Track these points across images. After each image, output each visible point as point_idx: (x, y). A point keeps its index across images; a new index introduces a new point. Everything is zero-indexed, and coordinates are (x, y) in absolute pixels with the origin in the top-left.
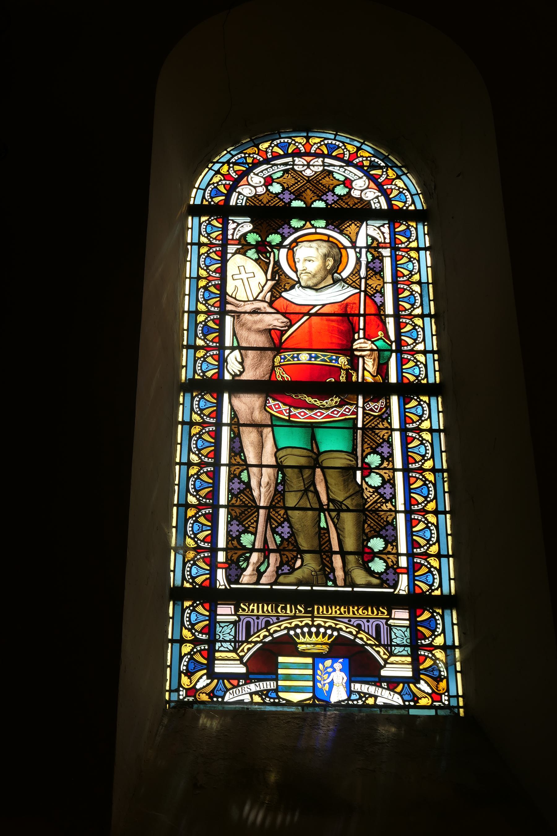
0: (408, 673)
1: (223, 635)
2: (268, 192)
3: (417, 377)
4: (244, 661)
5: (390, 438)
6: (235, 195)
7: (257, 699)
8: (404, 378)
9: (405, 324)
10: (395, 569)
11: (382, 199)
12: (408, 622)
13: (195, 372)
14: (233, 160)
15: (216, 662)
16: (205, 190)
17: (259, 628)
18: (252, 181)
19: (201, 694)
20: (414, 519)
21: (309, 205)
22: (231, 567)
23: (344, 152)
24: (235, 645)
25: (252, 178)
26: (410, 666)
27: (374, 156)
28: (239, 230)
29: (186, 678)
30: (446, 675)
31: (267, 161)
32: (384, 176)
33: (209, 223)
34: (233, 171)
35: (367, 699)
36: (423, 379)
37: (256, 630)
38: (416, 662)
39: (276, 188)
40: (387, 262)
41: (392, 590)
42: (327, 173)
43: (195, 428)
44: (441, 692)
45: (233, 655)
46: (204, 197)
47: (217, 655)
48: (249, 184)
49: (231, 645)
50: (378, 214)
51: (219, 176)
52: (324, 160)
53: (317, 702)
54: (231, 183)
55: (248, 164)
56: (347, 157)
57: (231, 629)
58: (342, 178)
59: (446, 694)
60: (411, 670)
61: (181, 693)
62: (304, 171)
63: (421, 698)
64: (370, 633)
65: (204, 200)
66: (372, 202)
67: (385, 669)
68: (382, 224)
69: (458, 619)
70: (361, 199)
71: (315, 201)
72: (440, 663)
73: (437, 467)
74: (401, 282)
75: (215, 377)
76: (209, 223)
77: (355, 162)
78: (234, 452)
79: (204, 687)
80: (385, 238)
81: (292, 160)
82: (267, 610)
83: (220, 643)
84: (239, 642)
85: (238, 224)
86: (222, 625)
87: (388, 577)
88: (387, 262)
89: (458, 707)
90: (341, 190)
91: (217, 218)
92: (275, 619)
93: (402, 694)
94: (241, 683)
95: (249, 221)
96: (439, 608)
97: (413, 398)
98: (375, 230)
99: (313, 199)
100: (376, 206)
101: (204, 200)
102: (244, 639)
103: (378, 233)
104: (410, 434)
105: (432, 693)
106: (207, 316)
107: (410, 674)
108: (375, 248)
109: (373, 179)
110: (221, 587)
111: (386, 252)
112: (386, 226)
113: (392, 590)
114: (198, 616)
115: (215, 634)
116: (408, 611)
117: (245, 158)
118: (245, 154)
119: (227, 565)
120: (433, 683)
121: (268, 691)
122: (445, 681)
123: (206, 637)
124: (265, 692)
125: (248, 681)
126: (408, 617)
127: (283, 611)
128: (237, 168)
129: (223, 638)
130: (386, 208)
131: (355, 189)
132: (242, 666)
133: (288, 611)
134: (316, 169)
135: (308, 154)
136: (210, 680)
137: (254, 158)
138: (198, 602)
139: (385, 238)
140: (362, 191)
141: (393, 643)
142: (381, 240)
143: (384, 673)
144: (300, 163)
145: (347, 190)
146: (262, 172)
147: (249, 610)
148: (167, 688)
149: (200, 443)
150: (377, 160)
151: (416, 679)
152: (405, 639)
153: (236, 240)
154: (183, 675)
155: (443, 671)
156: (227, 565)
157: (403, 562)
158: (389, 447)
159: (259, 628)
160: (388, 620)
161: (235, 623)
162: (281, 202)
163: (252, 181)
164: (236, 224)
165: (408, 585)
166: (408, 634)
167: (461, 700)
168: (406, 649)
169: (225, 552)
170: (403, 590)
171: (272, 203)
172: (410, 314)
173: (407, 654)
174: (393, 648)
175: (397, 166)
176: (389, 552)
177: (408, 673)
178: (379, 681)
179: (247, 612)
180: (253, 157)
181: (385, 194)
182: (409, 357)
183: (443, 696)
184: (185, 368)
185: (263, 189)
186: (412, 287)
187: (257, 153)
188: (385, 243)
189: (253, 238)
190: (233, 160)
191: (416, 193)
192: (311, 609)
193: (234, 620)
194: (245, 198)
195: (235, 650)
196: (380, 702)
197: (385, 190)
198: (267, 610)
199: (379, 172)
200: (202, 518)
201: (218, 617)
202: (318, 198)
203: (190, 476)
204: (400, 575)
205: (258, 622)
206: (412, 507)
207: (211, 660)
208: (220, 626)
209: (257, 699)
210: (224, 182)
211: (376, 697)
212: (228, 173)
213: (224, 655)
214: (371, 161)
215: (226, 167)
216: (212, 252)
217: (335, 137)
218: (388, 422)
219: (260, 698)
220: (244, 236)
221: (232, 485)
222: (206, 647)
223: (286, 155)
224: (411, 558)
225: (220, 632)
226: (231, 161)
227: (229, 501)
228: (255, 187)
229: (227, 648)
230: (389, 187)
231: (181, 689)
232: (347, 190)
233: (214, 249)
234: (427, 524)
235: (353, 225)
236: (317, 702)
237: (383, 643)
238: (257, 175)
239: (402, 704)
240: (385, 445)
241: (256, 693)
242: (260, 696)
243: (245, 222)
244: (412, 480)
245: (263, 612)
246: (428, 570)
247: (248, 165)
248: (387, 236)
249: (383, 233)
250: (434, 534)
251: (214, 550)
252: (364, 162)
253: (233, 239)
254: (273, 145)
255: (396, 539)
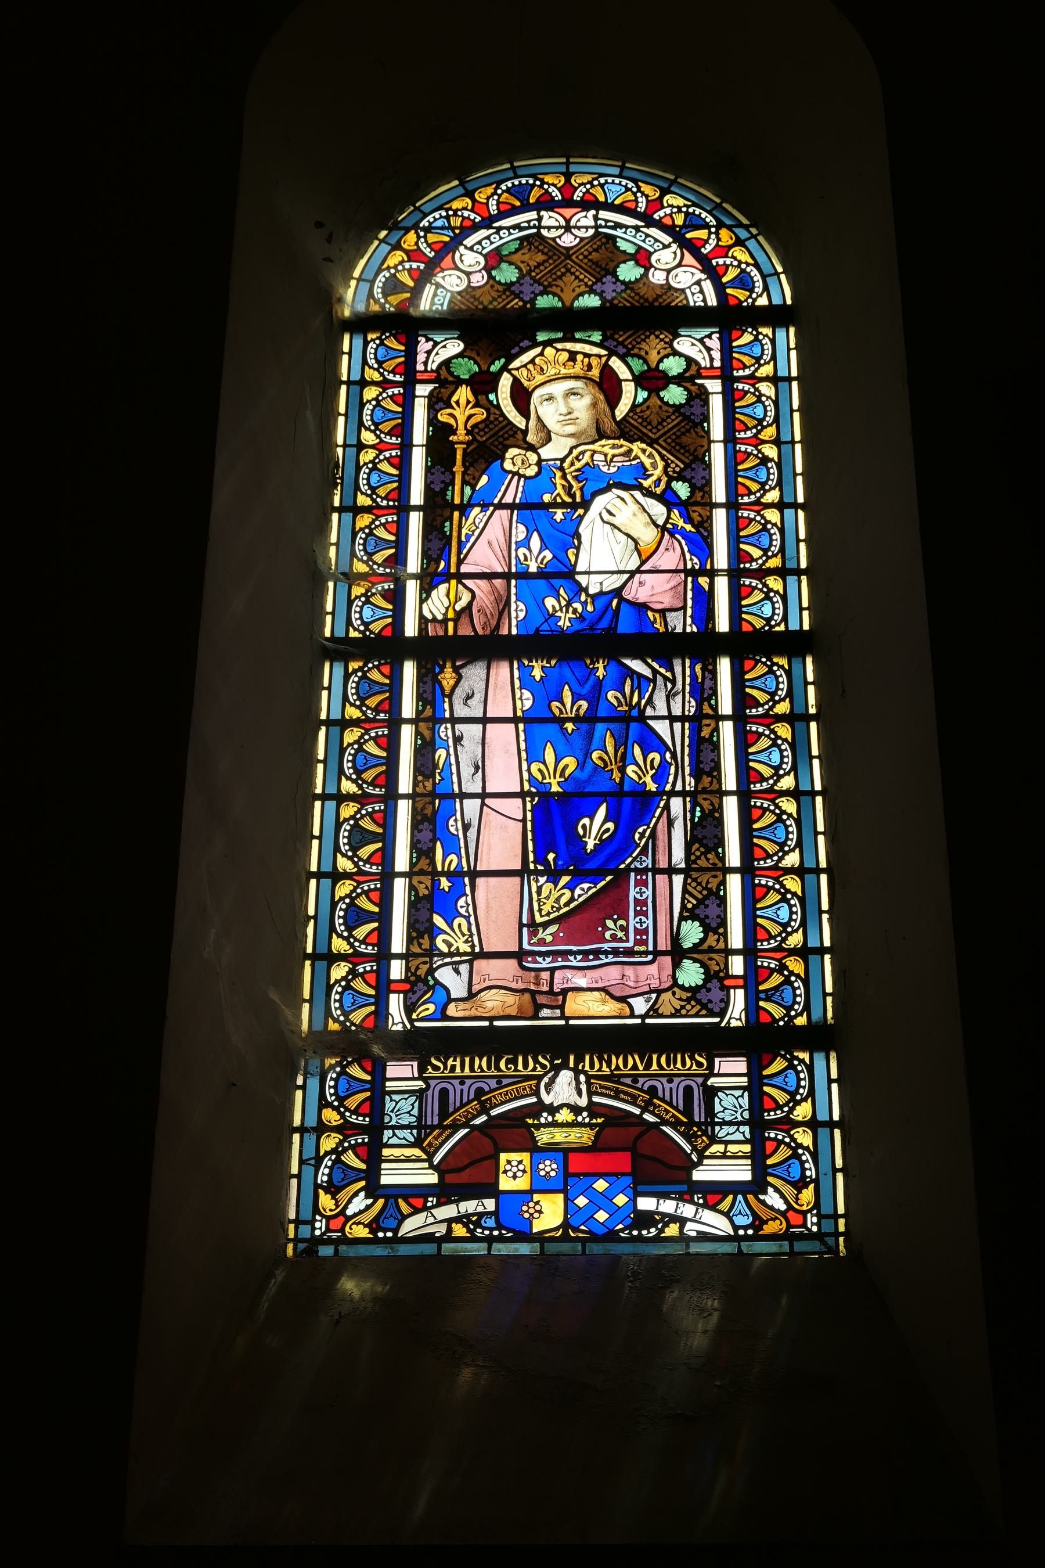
0: (743, 1173)
1: (397, 1116)
2: (491, 282)
3: (768, 620)
4: (435, 1163)
5: (715, 734)
6: (429, 290)
7: (459, 1230)
8: (762, 1013)
9: (775, 1144)
10: (721, 980)
11: (708, 286)
12: (745, 1079)
13: (349, 623)
14: (425, 223)
15: (384, 1166)
16: (372, 282)
17: (465, 1100)
18: (462, 261)
19: (354, 1227)
20: (760, 885)
21: (568, 304)
22: (415, 988)
23: (636, 198)
24: (419, 1133)
25: (461, 255)
26: (749, 1162)
27: (694, 204)
28: (437, 354)
29: (329, 1196)
30: (814, 1177)
31: (488, 222)
32: (713, 242)
33: (382, 343)
34: (425, 245)
35: (666, 1225)
36: (779, 625)
37: (458, 1104)
38: (758, 1158)
39: (507, 274)
40: (716, 404)
41: (717, 1020)
42: (604, 240)
43: (339, 965)
44: (805, 1208)
45: (417, 1152)
46: (371, 295)
47: (386, 1152)
48: (457, 268)
49: (411, 1133)
50: (698, 317)
51: (399, 253)
52: (597, 213)
53: (572, 1234)
54: (422, 266)
55: (453, 229)
56: (642, 206)
57: (412, 1105)
58: (631, 249)
59: (815, 1212)
60: (750, 1168)
61: (318, 1225)
62: (560, 237)
63: (768, 1220)
64: (675, 1103)
65: (351, 629)
66: (688, 291)
67: (700, 1168)
68: (707, 333)
69: (815, 671)
70: (668, 287)
71: (582, 294)
72: (804, 1154)
73: (780, 374)
74: (754, 720)
75: (388, 633)
76: (382, 343)
77: (656, 216)
78: (416, 930)
79: (361, 1212)
80: (712, 359)
81: (536, 217)
82: (480, 1067)
83: (391, 1131)
84: (426, 1127)
85: (436, 344)
86: (396, 1097)
87: (710, 995)
88: (716, 404)
89: (837, 1234)
90: (628, 272)
91: (380, 664)
92: (493, 1083)
93: (731, 1215)
94: (429, 1204)
95: (456, 336)
96: (803, 1050)
97: (760, 661)
98: (693, 344)
99: (578, 291)
100: (696, 299)
101: (351, 629)
102: (436, 1122)
103: (700, 351)
104: (740, 386)
105: (786, 1211)
106: (381, 390)
107: (746, 1176)
108: (692, 379)
109: (693, 247)
110: (394, 1028)
111: (714, 386)
112: (715, 336)
113: (717, 1020)
114: (352, 1084)
115: (383, 1114)
116: (745, 1059)
117: (448, 217)
118: (447, 210)
119: (407, 987)
120: (789, 1190)
121: (481, 1215)
122: (812, 1186)
123: (377, 869)
124: (474, 1219)
125: (443, 1200)
126: (745, 1071)
127: (509, 1066)
128: (432, 238)
129: (397, 1122)
130: (715, 304)
131: (656, 269)
132: (431, 1171)
133: (520, 1067)
134: (582, 233)
135: (568, 202)
136: (371, 1200)
137: (464, 218)
138: (387, 334)
139: (712, 359)
140: (669, 271)
141: (716, 1120)
142: (705, 363)
143: (698, 1175)
144: (552, 223)
145: (642, 271)
146: (479, 243)
147: (445, 1068)
148: (292, 1215)
149: (374, 478)
150: (698, 211)
151: (758, 1185)
152: (740, 1111)
153: (432, 371)
154: (321, 1192)
155: (810, 1169)
156: (407, 987)
157: (737, 966)
158: (719, 906)
159: (465, 1100)
160: (707, 1077)
161: (420, 1094)
162: (517, 300)
163: (462, 261)
164: (431, 343)
165: (747, 1009)
166: (745, 1102)
167: (842, 1222)
168: (742, 1128)
169: (411, 801)
170: (737, 1019)
171: (499, 303)
172: (775, 867)
173: (743, 1139)
174: (717, 1128)
175: (740, 225)
176: (710, 947)
177: (743, 1173)
178: (691, 1191)
179: (443, 1072)
180: (462, 216)
181: (714, 274)
182: (760, 730)
183: (809, 1215)
184: (312, 921)
185: (483, 277)
186: (763, 450)
187: (469, 207)
188: (712, 367)
189: (466, 368)
190: (425, 223)
191: (773, 271)
192: (559, 1061)
193: (417, 1088)
194: (449, 294)
195: (417, 1144)
196: (691, 1230)
197: (714, 268)
198: (480, 1067)
199: (702, 234)
200: (367, 819)
201: (388, 1084)
202: (587, 289)
203: (322, 1154)
204: (732, 991)
205: (462, 1090)
206: (759, 944)
207: (374, 1159)
208: (392, 1100)
209: (459, 1230)
210: (407, 265)
211: (682, 1221)
212: (415, 247)
213: (397, 1152)
214: (687, 214)
215: (411, 237)
216: (379, 526)
217: (621, 172)
218: (710, 706)
219: (465, 1230)
220: (447, 363)
221: (412, 996)
222: (378, 886)
223: (526, 207)
224: (733, 511)
225: (392, 1111)
226: (421, 225)
227: (412, 865)
228: (468, 274)
229: (404, 1138)
230: (721, 261)
231: (318, 1217)
232: (642, 271)
233: (383, 520)
234: (794, 1150)
235: (652, 337)
236: (572, 1234)
237: (697, 1119)
238: (471, 249)
239: (732, 1233)
240: (712, 902)
241: (457, 1220)
242: (466, 1225)
243: (446, 339)
244: (770, 1146)
245: (472, 1069)
246: (780, 897)
247: (454, 232)
248: (717, 355)
249: (709, 349)
250: (792, 833)
251: (384, 956)
252: (674, 215)
253: (426, 371)
254: (499, 192)
255: (723, 922)
